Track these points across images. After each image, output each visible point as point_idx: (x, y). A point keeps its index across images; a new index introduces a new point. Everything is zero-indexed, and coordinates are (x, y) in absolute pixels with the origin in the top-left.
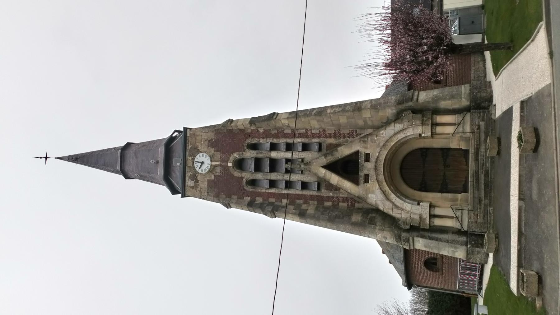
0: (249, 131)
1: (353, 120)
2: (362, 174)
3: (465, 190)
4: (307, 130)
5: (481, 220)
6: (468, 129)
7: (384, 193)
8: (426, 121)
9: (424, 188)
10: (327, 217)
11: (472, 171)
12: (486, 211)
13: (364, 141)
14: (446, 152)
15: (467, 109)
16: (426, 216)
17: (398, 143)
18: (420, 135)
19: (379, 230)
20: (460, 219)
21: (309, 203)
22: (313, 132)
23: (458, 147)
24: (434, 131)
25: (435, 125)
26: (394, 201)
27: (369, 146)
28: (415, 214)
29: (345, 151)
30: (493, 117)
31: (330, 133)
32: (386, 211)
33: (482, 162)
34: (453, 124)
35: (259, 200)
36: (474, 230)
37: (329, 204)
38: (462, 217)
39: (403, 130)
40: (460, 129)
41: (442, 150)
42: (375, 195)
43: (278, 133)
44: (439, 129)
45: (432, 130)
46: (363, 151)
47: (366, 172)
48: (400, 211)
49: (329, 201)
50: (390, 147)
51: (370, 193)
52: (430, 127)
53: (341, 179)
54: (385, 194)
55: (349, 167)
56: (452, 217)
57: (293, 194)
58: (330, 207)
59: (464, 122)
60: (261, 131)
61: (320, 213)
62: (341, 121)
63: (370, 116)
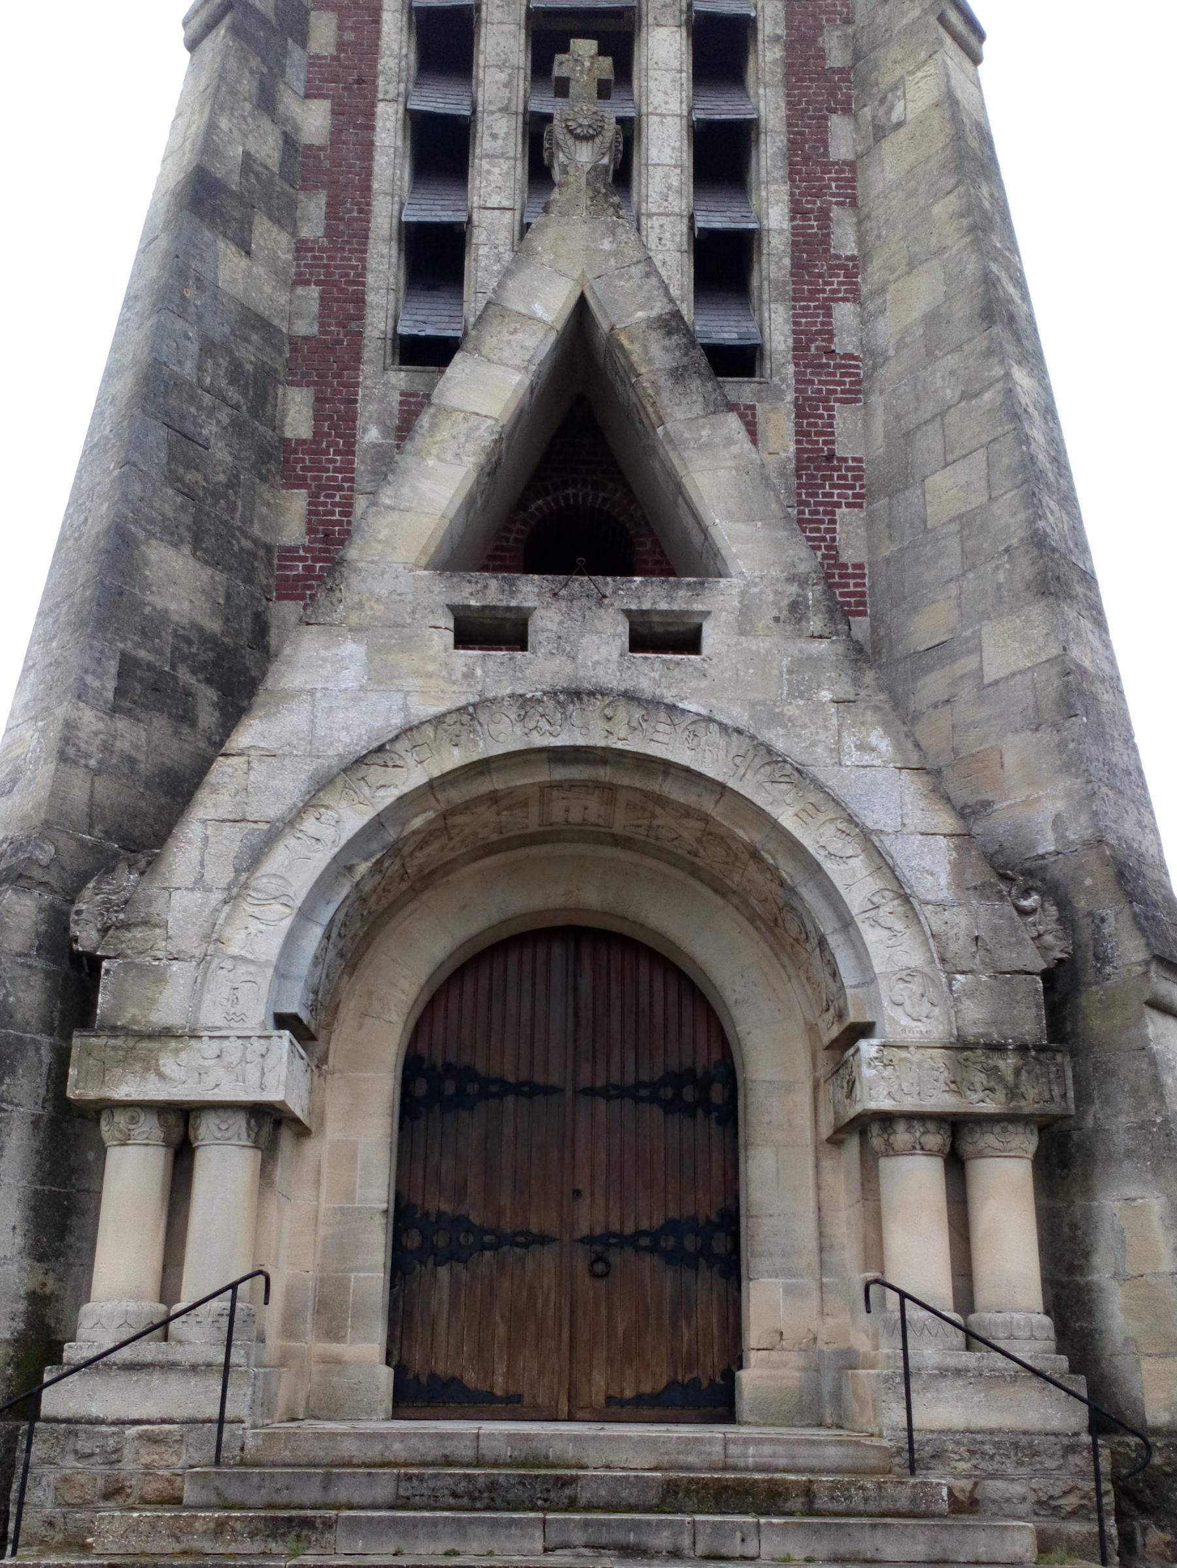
1: (952, 563)
2: (529, 591)
3: (414, 1393)
4: (852, 269)
6: (942, 1411)
7: (379, 753)
9: (430, 1092)
10: (188, 369)
11: (570, 1452)
13: (796, 608)
14: (713, 1245)
15: (1107, 1416)
16: (179, 1078)
17: (788, 869)
19: (69, 725)
20: (148, 1350)
21: (301, 281)
22: (844, 313)
23: (754, 1335)
24: (902, 1136)
25: (956, 1141)
26: (309, 825)
27: (759, 644)
28: (198, 988)
32: (223, 770)
33: (662, 1540)
34: (965, 1296)
36: (50, 1475)
37: (297, 415)
38: (169, 1367)
39: (906, 899)
40: (933, 1349)
42: (370, 692)
43: (825, 74)
44: (916, 1179)
45: (912, 1117)
46: (719, 608)
47: (546, 622)
48: (220, 874)
49: (318, 418)
50: (760, 800)
51: (374, 650)
52: (941, 1101)
53: (485, 435)
54: (360, 761)
55: (578, 501)
58: (275, 424)
61: (219, 330)
62: (940, 481)
63: (992, 672)
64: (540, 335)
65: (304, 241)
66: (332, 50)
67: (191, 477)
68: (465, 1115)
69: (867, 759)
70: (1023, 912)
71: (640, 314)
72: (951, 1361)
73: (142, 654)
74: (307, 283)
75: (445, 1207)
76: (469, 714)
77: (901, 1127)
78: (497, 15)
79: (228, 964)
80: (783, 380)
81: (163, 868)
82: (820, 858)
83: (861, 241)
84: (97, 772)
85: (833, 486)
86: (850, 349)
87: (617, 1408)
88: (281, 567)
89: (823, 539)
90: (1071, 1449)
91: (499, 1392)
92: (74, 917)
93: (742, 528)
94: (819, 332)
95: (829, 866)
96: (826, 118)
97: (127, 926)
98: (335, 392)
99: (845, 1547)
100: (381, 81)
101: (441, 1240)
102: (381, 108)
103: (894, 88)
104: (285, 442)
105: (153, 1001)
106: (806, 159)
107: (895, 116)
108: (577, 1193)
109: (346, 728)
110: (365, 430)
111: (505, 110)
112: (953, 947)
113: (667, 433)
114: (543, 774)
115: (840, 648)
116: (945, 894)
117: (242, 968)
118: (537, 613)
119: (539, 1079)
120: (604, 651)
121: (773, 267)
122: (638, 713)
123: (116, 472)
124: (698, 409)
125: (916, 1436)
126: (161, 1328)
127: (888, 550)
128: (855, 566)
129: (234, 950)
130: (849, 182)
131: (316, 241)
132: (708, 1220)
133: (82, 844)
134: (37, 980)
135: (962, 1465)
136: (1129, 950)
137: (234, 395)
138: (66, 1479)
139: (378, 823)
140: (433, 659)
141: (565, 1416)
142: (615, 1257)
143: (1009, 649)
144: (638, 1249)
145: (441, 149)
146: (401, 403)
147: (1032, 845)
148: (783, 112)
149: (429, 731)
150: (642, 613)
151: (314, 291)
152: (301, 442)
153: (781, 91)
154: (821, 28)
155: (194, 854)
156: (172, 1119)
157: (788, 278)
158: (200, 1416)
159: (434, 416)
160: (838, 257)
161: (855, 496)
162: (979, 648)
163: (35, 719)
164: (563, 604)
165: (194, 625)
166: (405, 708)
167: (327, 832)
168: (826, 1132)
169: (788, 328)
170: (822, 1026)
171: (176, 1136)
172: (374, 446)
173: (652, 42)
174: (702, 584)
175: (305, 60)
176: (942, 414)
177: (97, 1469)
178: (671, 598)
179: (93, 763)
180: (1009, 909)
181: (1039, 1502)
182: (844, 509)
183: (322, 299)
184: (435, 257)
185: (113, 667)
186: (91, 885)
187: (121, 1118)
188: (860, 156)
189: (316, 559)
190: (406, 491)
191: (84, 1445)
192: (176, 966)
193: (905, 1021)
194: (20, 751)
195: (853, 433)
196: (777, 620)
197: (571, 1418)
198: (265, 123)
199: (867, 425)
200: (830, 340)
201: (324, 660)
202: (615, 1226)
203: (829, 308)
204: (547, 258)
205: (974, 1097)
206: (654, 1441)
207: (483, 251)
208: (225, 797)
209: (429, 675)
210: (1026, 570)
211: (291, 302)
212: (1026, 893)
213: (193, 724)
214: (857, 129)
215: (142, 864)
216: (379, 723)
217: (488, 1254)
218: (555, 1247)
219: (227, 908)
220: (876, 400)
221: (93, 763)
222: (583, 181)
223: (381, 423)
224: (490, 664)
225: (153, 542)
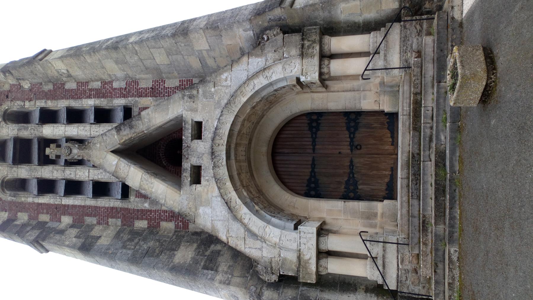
0: (7, 87)
1: (179, 57)
2: (186, 165)
3: (391, 195)
4: (104, 83)
5: (426, 271)
6: (395, 60)
7: (227, 203)
8: (309, 47)
9: (314, 190)
10: (130, 252)
11: (406, 155)
12: (440, 253)
14: (353, 118)
16: (310, 255)
17: (257, 99)
18: (298, 80)
19: (220, 282)
20: (380, 262)
21: (107, 223)
22: (116, 85)
23: (376, 108)
24: (325, 70)
25: (326, 56)
26: (246, 221)
27: (200, 106)
28: (287, 250)
29: (155, 117)
30: (457, 15)
31: (144, 86)
33: (428, 131)
34: (365, 54)
35: (23, 217)
36: (412, 287)
37: (141, 224)
38: (384, 257)
39: (265, 69)
40: (379, 62)
41: (347, 114)
43: (55, 90)
44: (336, 67)
45: (320, 67)
47: (194, 161)
48: (258, 244)
49: (142, 219)
50: (239, 106)
51: (201, 205)
53: (146, 176)
54: (229, 208)
55: (163, 153)
56: (364, 257)
57: (80, 206)
58: (144, 230)
59: (387, 46)
60: (26, 85)
61: (120, 244)
63: (207, 47)
64: (121, 162)
65: (97, 223)
66: (48, 215)
67: (157, 251)
68: (320, 182)
69: (229, 79)
70: (268, 39)
71: (116, 137)
72: (382, 58)
73: (202, 264)
74: (108, 222)
75: (343, 187)
76: (218, 180)
77: (323, 70)
79: (281, 242)
80: (133, 100)
81: (257, 258)
82: (254, 91)
83: (97, 81)
84: (232, 275)
85: (160, 88)
86: (125, 83)
88: (180, 228)
91: (390, 173)
95: (257, 88)
96: (66, 90)
97: (272, 268)
98: (136, 215)
100: (56, 203)
101: (352, 188)
102: (63, 203)
103: (58, 72)
104: (148, 227)
105: (291, 261)
107: (65, 72)
109: (221, 212)
110: (145, 207)
111: (64, 172)
112: (277, 57)
113: (146, 130)
114: (233, 162)
115: (201, 86)
117: (282, 238)
119: (310, 163)
120: (201, 146)
121: (104, 103)
122: (217, 137)
124: (140, 122)
126: (374, 259)
127: (176, 74)
128: (180, 82)
129: (278, 240)
130: (82, 84)
132: (347, 119)
135: (409, 55)
137: (136, 240)
138: (413, 283)
140: (204, 190)
142: (356, 143)
144: (354, 137)
145: (74, 188)
147: (251, 37)
148: (64, 100)
152: (148, 223)
153: (59, 101)
154: (43, 91)
156: (321, 256)
158: (396, 249)
159: (142, 189)
160: (101, 86)
161: (162, 82)
162: (201, 51)
163: (219, 291)
165: (195, 251)
166: (216, 197)
167: (248, 217)
168: (324, 90)
169: (119, 99)
170: (297, 90)
171: (325, 255)
175: (51, 222)
176: (141, 60)
178: (188, 129)
179: (230, 276)
180: (267, 43)
181: (418, 35)
183: (112, 218)
184: (101, 189)
187: (321, 269)
189: (178, 220)
190: (161, 197)
191: (404, 279)
192: (282, 255)
193: (296, 69)
195: (146, 83)
196: (193, 102)
197: (397, 155)
198: (67, 232)
199: (144, 79)
200: (122, 88)
201: (204, 217)
202: (348, 143)
205: (315, 52)
206: (403, 133)
208: (239, 243)
209: (208, 191)
210: (181, 39)
212: (263, 39)
213: (220, 251)
214: (68, 81)
215: (256, 264)
216: (220, 203)
217: (355, 176)
218: (353, 159)
219: (267, 242)
220: (138, 77)
221: (230, 276)
224: (205, 175)
225: (174, 261)
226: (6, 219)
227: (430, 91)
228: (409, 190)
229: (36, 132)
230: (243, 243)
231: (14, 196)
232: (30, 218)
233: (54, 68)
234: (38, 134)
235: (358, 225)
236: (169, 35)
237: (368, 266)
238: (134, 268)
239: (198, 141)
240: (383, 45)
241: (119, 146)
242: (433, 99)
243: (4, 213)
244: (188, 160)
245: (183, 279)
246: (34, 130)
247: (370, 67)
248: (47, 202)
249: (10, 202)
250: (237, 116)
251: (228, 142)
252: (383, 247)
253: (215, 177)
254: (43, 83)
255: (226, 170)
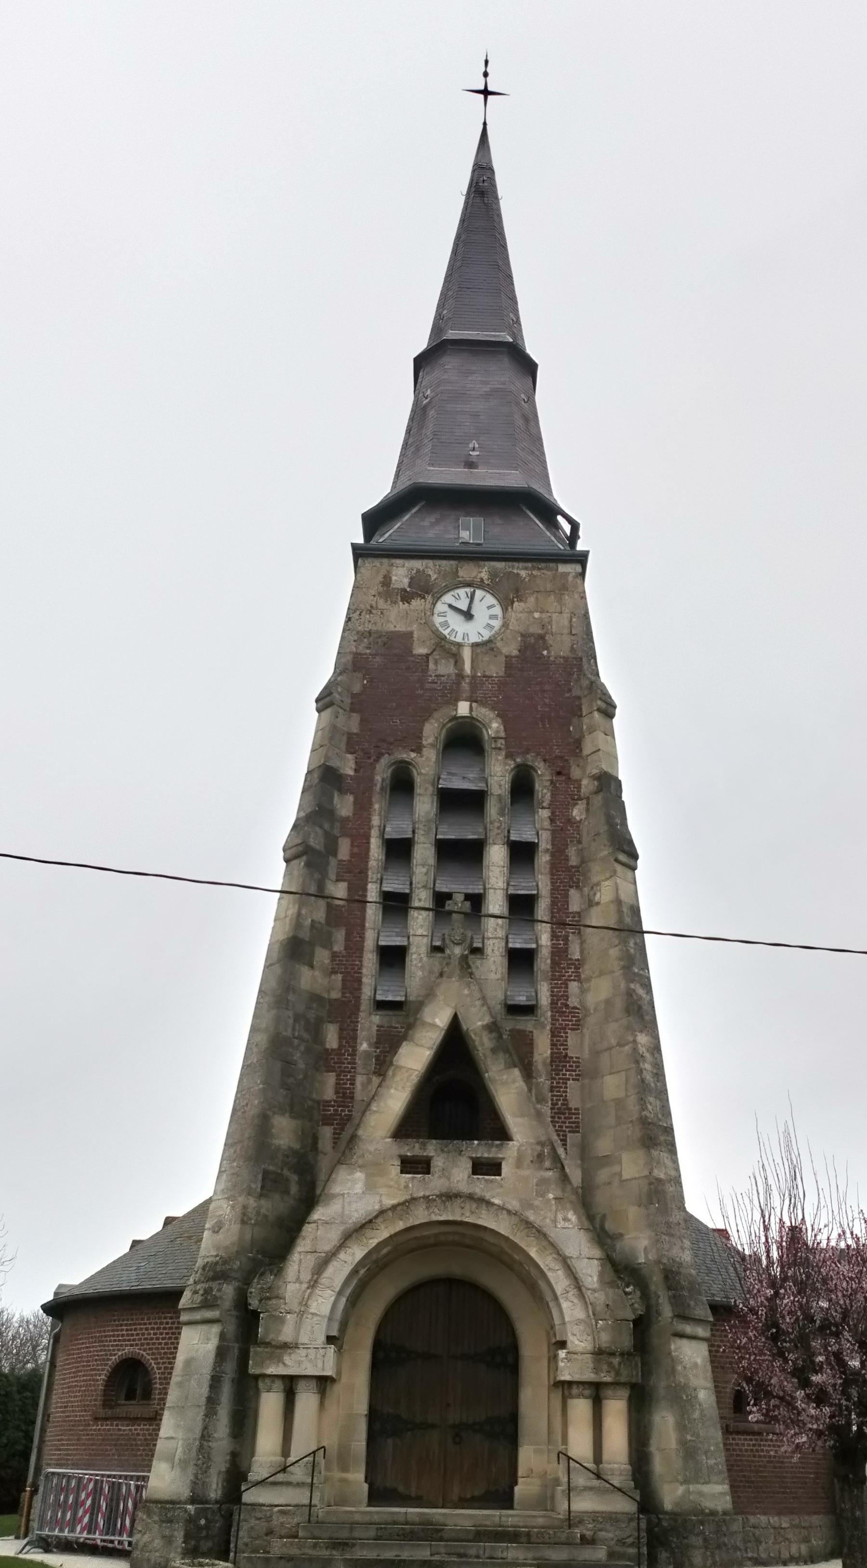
0: (576, 773)
1: (611, 1120)
2: (431, 1149)
3: (377, 1496)
4: (578, 965)
6: (583, 1504)
8: (610, 1364)
9: (385, 1359)
11: (441, 1519)
14: (506, 1430)
16: (291, 1365)
19: (245, 1207)
20: (280, 1477)
21: (334, 972)
22: (573, 986)
23: (521, 1471)
24: (575, 1391)
25: (597, 1393)
26: (342, 1256)
27: (526, 1172)
29: (508, 1092)
32: (308, 1230)
33: (473, 1552)
34: (598, 1457)
35: (344, 806)
36: (245, 1526)
37: (332, 1038)
38: (288, 1484)
40: (581, 1480)
41: (513, 1418)
43: (569, 869)
44: (581, 1408)
45: (579, 1383)
46: (509, 1154)
47: (438, 1162)
48: (306, 1276)
49: (341, 1038)
50: (522, 1245)
51: (369, 1176)
53: (415, 1078)
55: (453, 1105)
56: (286, 1451)
57: (363, 919)
58: (322, 1043)
59: (606, 1491)
60: (577, 813)
61: (301, 1008)
63: (626, 1176)
64: (438, 1033)
65: (335, 952)
69: (567, 1225)
70: (626, 1294)
71: (480, 1023)
72: (589, 1484)
73: (271, 1168)
74: (336, 973)
77: (575, 1387)
78: (422, 839)
79: (310, 1316)
80: (546, 1019)
81: (284, 1274)
82: (545, 1270)
83: (582, 952)
84: (255, 1225)
86: (576, 1004)
87: (464, 1503)
88: (324, 1110)
89: (561, 1096)
90: (631, 1520)
91: (413, 1495)
92: (249, 1295)
93: (519, 1120)
94: (562, 996)
95: (549, 1274)
96: (568, 890)
97: (269, 1298)
98: (349, 1026)
99: (539, 1554)
100: (370, 873)
102: (370, 886)
104: (327, 1050)
105: (280, 1331)
106: (559, 910)
108: (448, 1405)
109: (356, 1211)
110: (361, 1044)
111: (425, 887)
112: (598, 1309)
113: (489, 1077)
114: (436, 1230)
115: (557, 1175)
116: (596, 1286)
117: (315, 1318)
118: (435, 1158)
121: (543, 965)
122: (474, 1206)
123: (261, 1086)
124: (502, 1066)
125: (572, 1514)
126: (284, 1470)
127: (588, 1105)
128: (575, 1109)
129: (312, 1311)
130: (578, 925)
131: (340, 952)
133: (249, 1258)
134: (234, 1320)
135: (590, 1526)
136: (667, 1311)
137: (306, 1036)
138: (252, 1528)
139: (370, 1253)
140: (392, 1180)
141: (441, 1505)
143: (631, 1166)
146: (378, 1031)
147: (637, 1258)
148: (549, 887)
149: (390, 1213)
150: (477, 1158)
151: (340, 977)
152: (332, 1050)
153: (549, 876)
154: (567, 845)
155: (296, 1267)
157: (549, 969)
159: (394, 1070)
160: (571, 959)
161: (576, 1075)
162: (620, 1163)
163: (228, 1199)
164: (445, 1155)
165: (290, 1148)
166: (380, 1201)
167: (349, 1259)
168: (552, 1383)
169: (548, 994)
172: (365, 1051)
173: (491, 853)
174: (502, 1145)
177: (263, 1524)
178: (489, 1152)
180: (620, 1292)
181: (618, 1540)
182: (571, 1081)
183: (343, 980)
185: (260, 1177)
186: (255, 1281)
187: (268, 1381)
188: (582, 910)
189: (339, 1106)
190: (382, 1104)
191: (259, 1515)
192: (289, 1316)
193: (577, 1342)
194: (221, 1213)
196: (532, 1161)
197: (442, 1507)
199: (582, 1041)
200: (567, 1000)
201: (348, 1180)
203: (567, 985)
204: (441, 998)
205: (603, 1375)
206: (474, 1515)
207: (414, 956)
208: (308, 1241)
209: (390, 1187)
210: (638, 1134)
211: (329, 982)
212: (628, 1286)
215: (275, 1271)
216: (370, 1208)
217: (409, 1433)
219: (309, 1291)
221: (253, 1221)
222: (457, 963)
223: (368, 1040)
226: (342, 771)
227: (530, 1555)
228: (390, 1524)
229: (496, 831)
230: (308, 1249)
231: (382, 789)
232: (345, 820)
233: (603, 881)
234: (492, 834)
235: (331, 1441)
236: (644, 1113)
237: (273, 1459)
238: (262, 1039)
239: (470, 1170)
240: (608, 1485)
241: (465, 1028)
242: (518, 1559)
243: (353, 766)
244: (439, 1151)
245: (247, 1135)
246: (498, 828)
247: (572, 1463)
248: (371, 854)
249: (371, 779)
250: (507, 1239)
251: (467, 1223)
252: (303, 1483)
253: (413, 1200)
254: (580, 846)
255: (423, 1221)
